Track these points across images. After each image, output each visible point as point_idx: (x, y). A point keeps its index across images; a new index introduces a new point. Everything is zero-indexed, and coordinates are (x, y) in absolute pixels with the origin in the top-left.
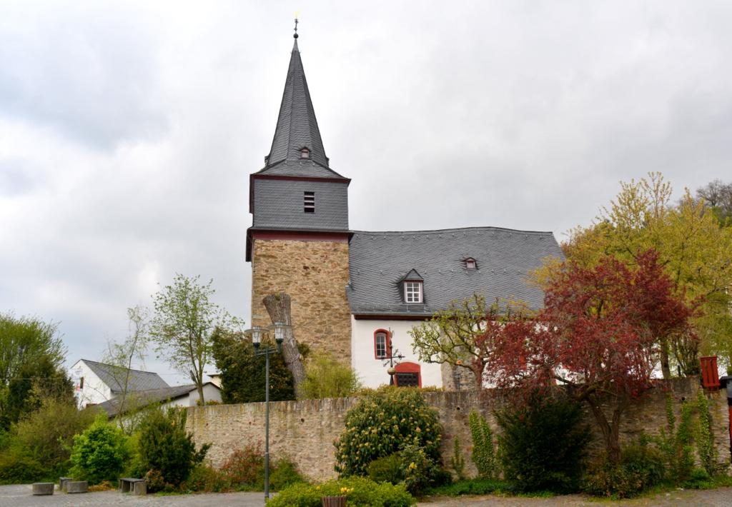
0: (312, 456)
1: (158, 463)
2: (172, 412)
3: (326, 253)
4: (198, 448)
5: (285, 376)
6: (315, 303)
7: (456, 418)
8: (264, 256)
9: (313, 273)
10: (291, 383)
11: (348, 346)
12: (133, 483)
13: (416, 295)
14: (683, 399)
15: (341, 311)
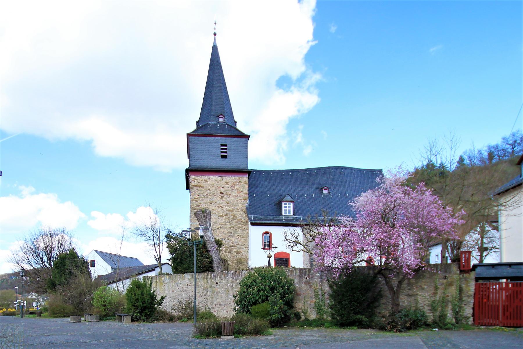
0: (222, 303)
1: (136, 306)
2: (144, 278)
3: (234, 184)
4: (159, 298)
5: (208, 258)
6: (227, 215)
7: (305, 283)
8: (196, 186)
9: (226, 197)
10: (211, 262)
11: (247, 241)
12: (124, 316)
13: (289, 211)
14: (446, 277)
15: (243, 220)
